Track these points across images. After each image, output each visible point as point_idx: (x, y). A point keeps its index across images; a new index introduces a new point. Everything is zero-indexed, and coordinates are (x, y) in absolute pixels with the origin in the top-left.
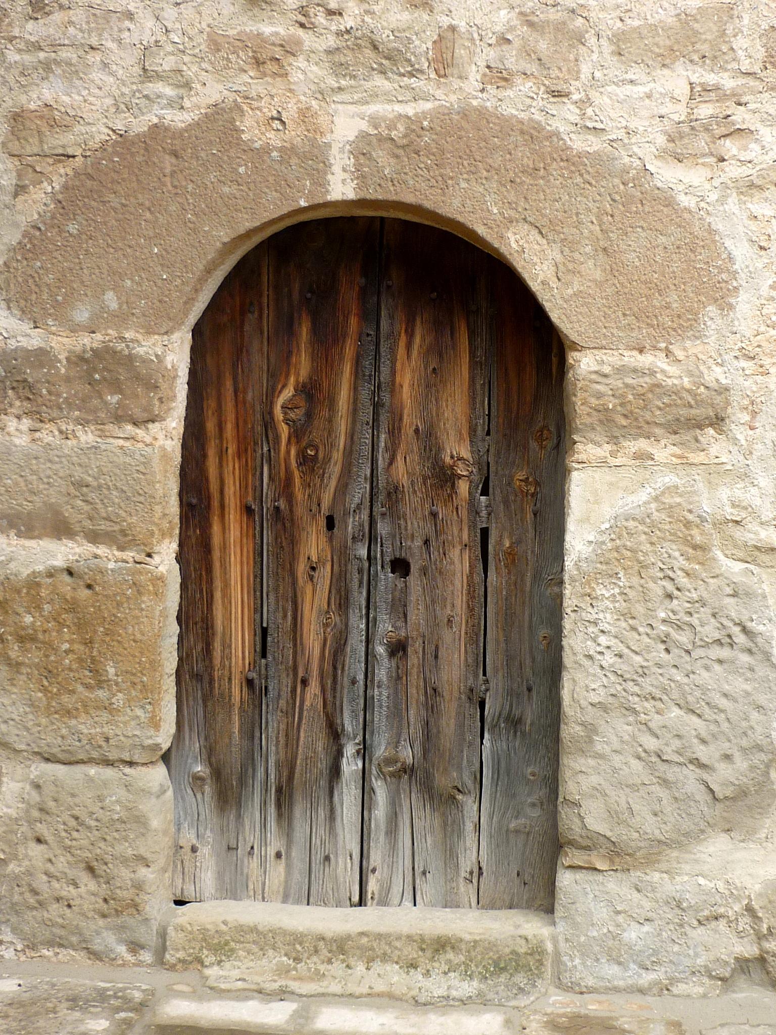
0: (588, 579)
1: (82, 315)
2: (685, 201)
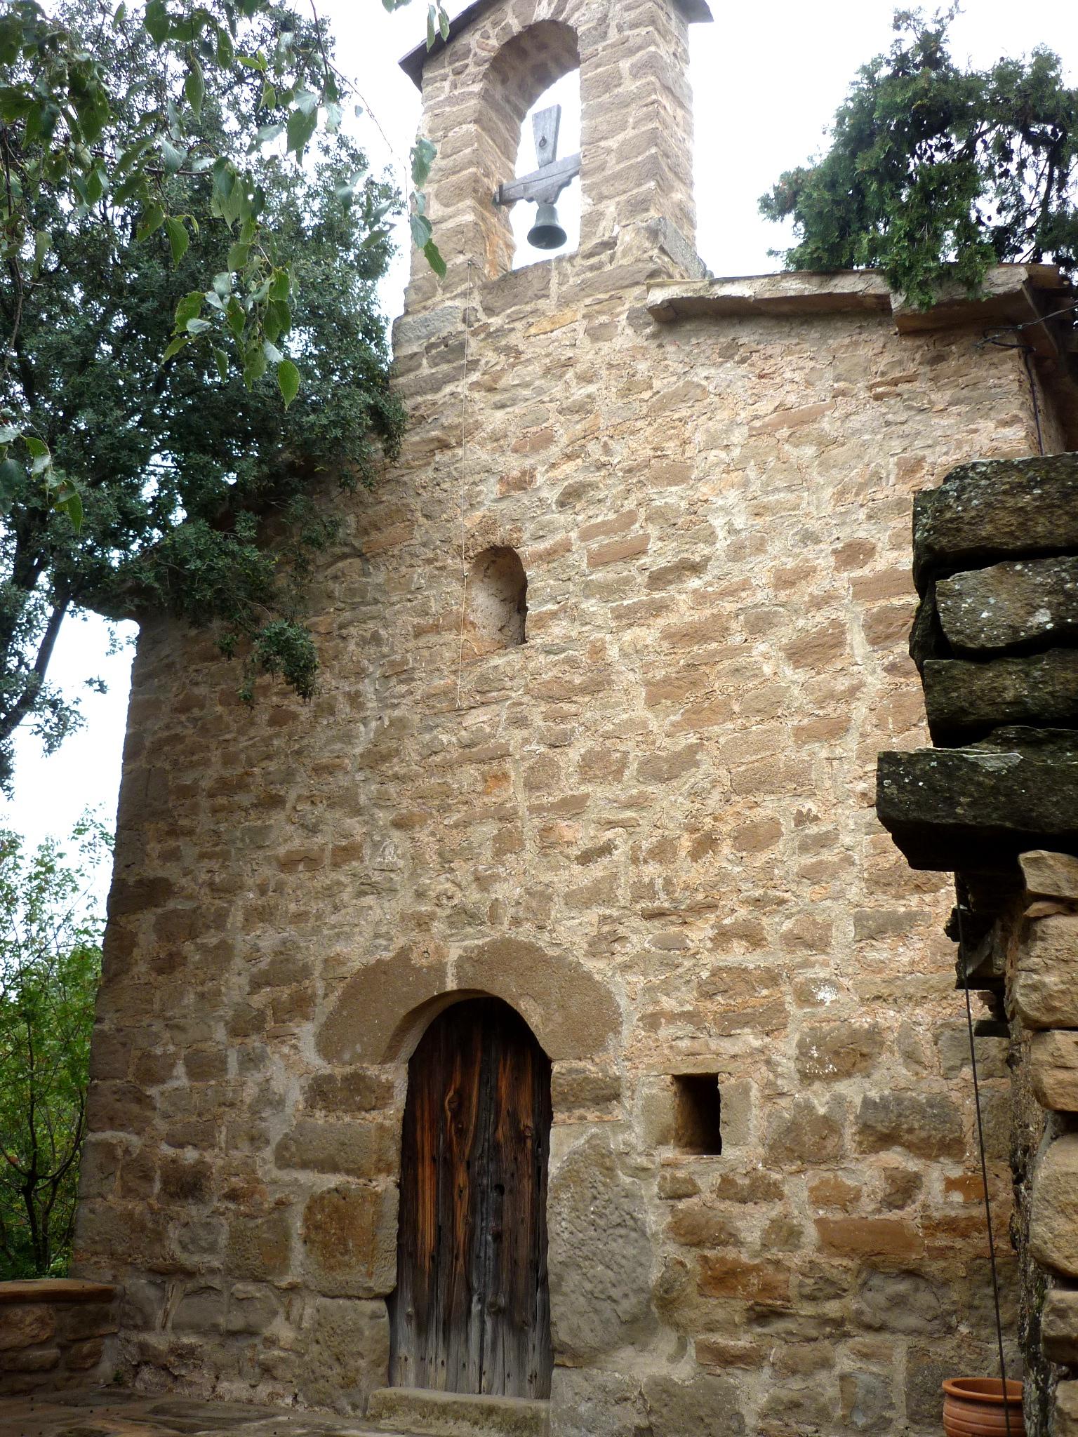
0: (557, 1189)
1: (347, 1056)
2: (597, 977)
